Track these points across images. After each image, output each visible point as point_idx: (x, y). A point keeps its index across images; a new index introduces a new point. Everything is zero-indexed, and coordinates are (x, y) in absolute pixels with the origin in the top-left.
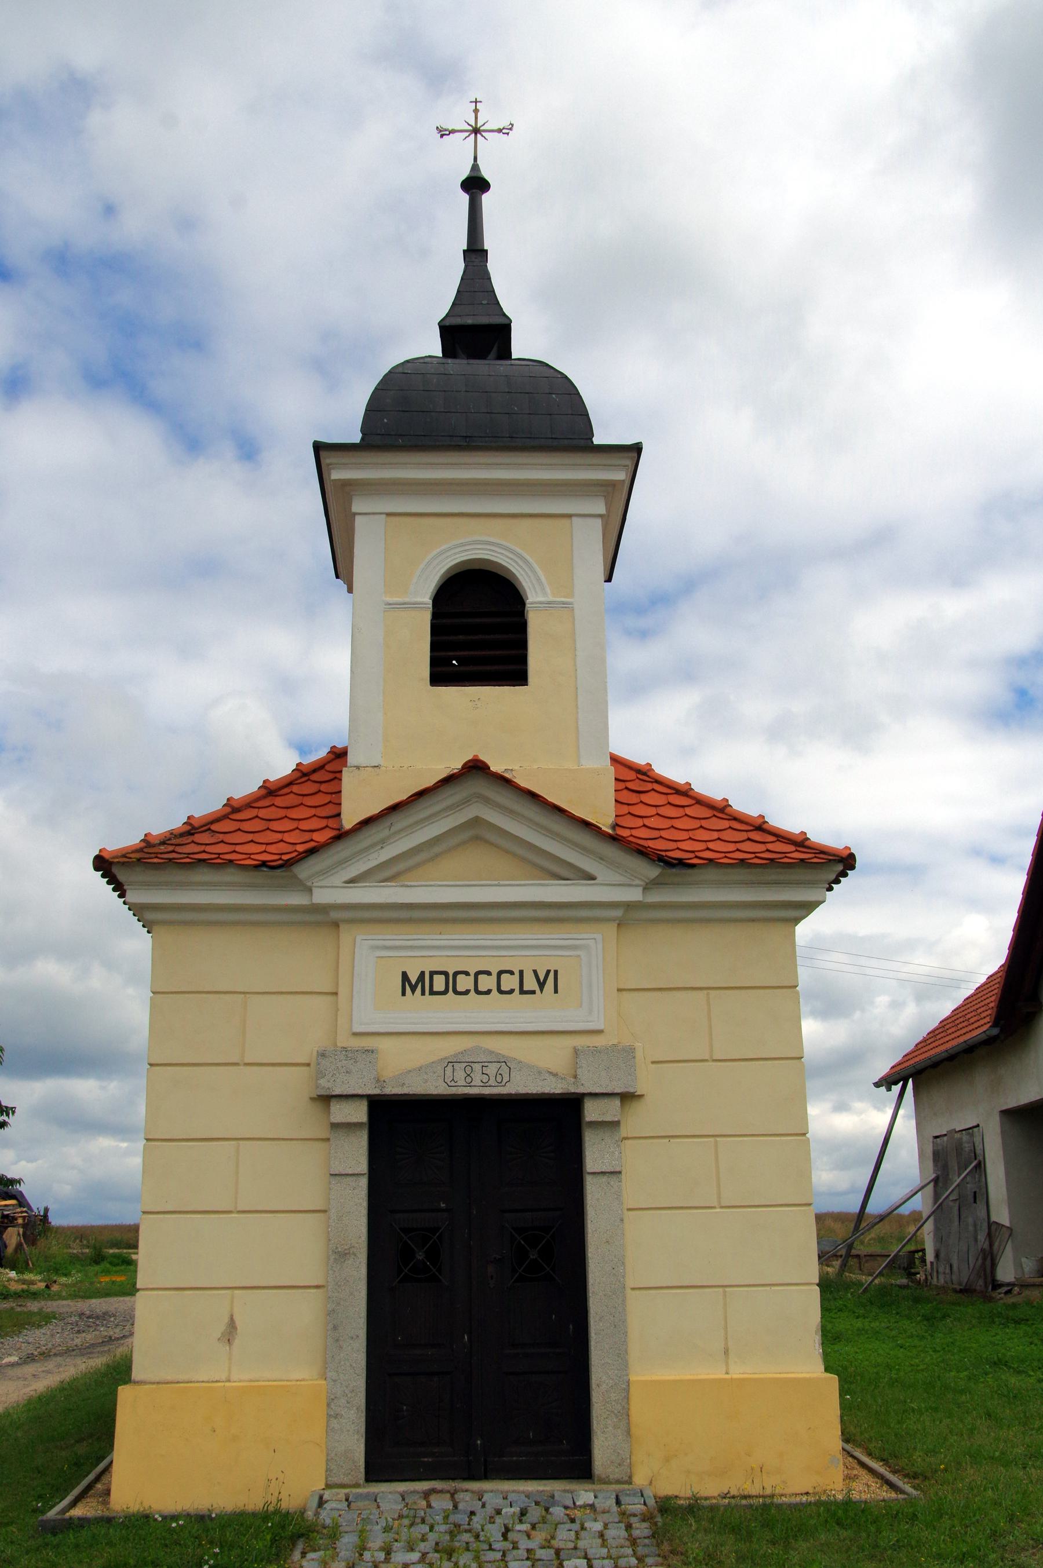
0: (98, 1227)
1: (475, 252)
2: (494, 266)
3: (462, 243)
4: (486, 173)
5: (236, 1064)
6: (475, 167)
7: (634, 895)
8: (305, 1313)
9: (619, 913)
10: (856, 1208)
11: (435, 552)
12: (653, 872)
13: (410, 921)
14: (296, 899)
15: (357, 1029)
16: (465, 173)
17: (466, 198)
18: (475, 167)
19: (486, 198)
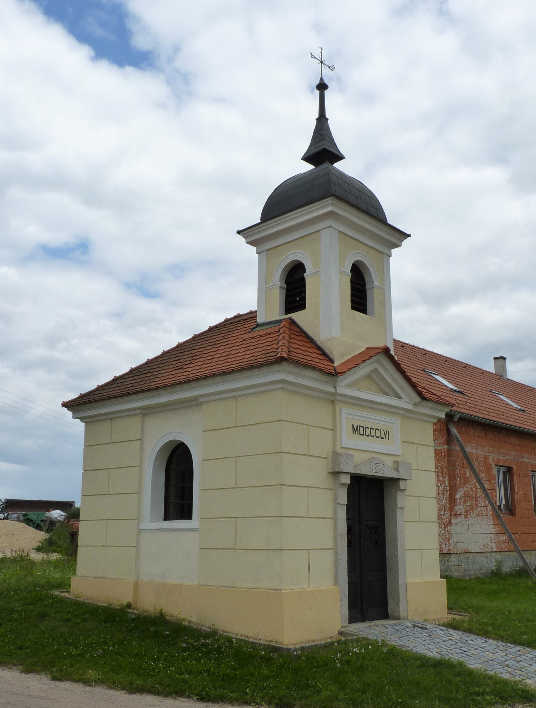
0: (398, 579)
1: (322, 119)
2: (332, 124)
3: (316, 114)
4: (326, 81)
5: (306, 455)
6: (321, 79)
7: (410, 407)
8: (328, 558)
9: (402, 412)
10: (330, 491)
11: (293, 252)
12: (418, 399)
13: (356, 405)
14: (330, 389)
15: (344, 446)
16: (318, 82)
17: (317, 92)
18: (321, 79)
19: (326, 92)
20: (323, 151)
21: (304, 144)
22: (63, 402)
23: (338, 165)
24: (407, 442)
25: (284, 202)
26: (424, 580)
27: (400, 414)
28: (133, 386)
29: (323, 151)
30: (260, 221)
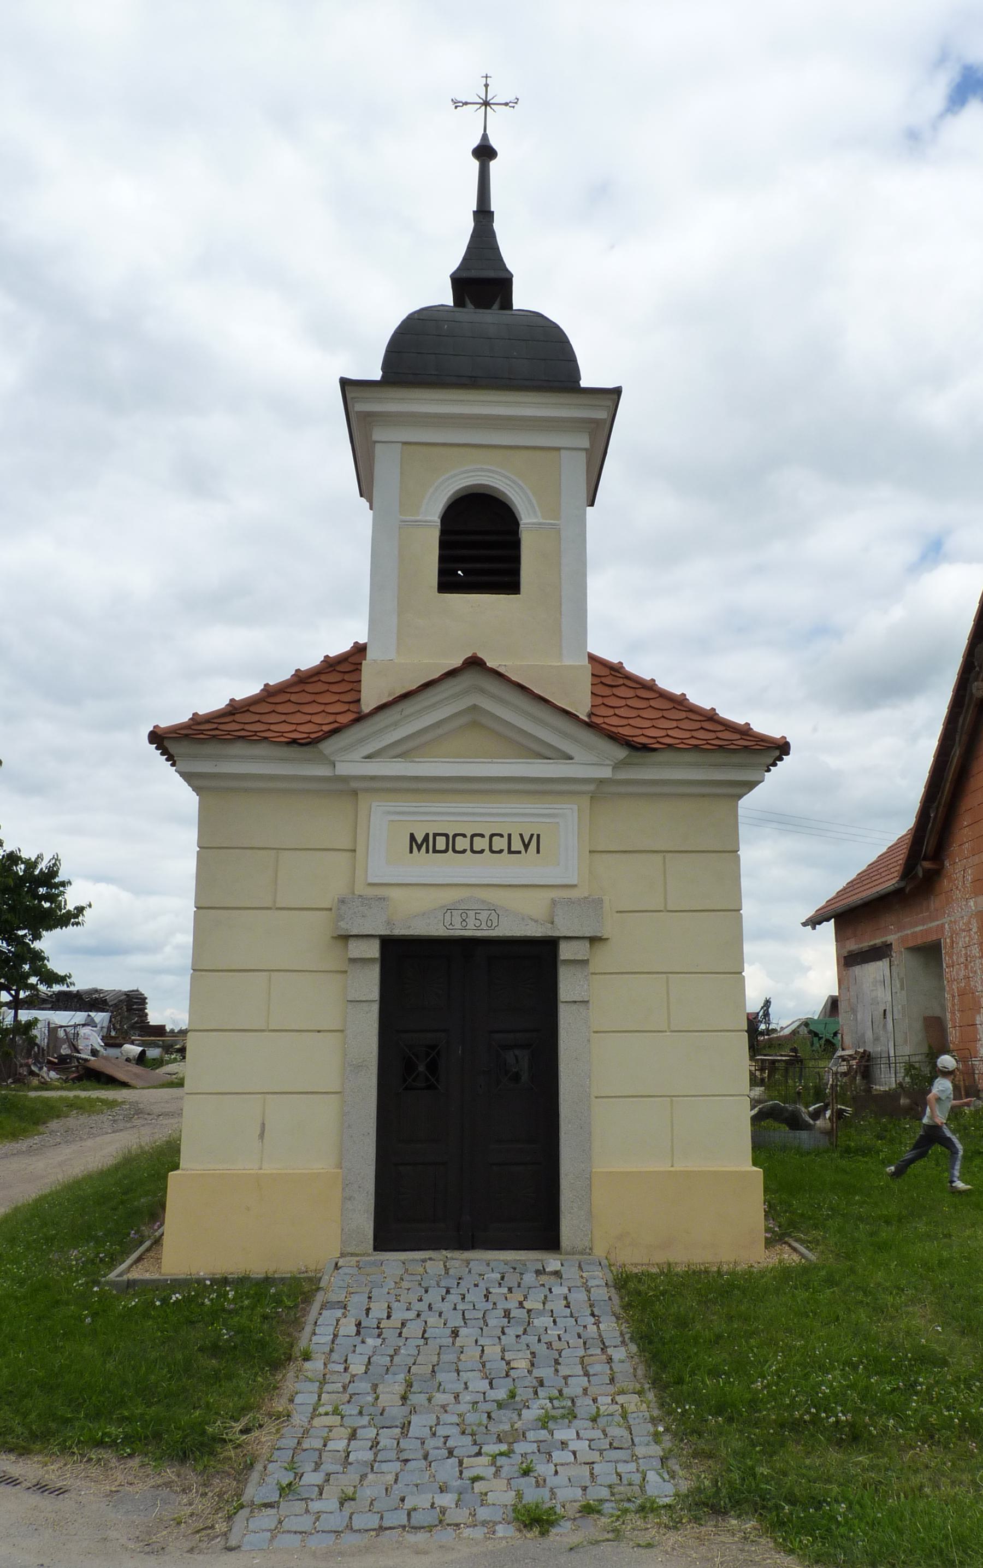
1: (484, 215)
2: (498, 226)
4: (494, 143)
6: (485, 137)
12: (621, 753)
13: (425, 791)
16: (476, 142)
17: (476, 164)
18: (485, 137)
19: (493, 164)
20: (483, 279)
21: (454, 254)
22: (327, 657)
23: (50, 943)
24: (625, 852)
25: (420, 355)
26: (678, 1167)
27: (584, 793)
28: (217, 729)
29: (483, 279)
30: (378, 378)
